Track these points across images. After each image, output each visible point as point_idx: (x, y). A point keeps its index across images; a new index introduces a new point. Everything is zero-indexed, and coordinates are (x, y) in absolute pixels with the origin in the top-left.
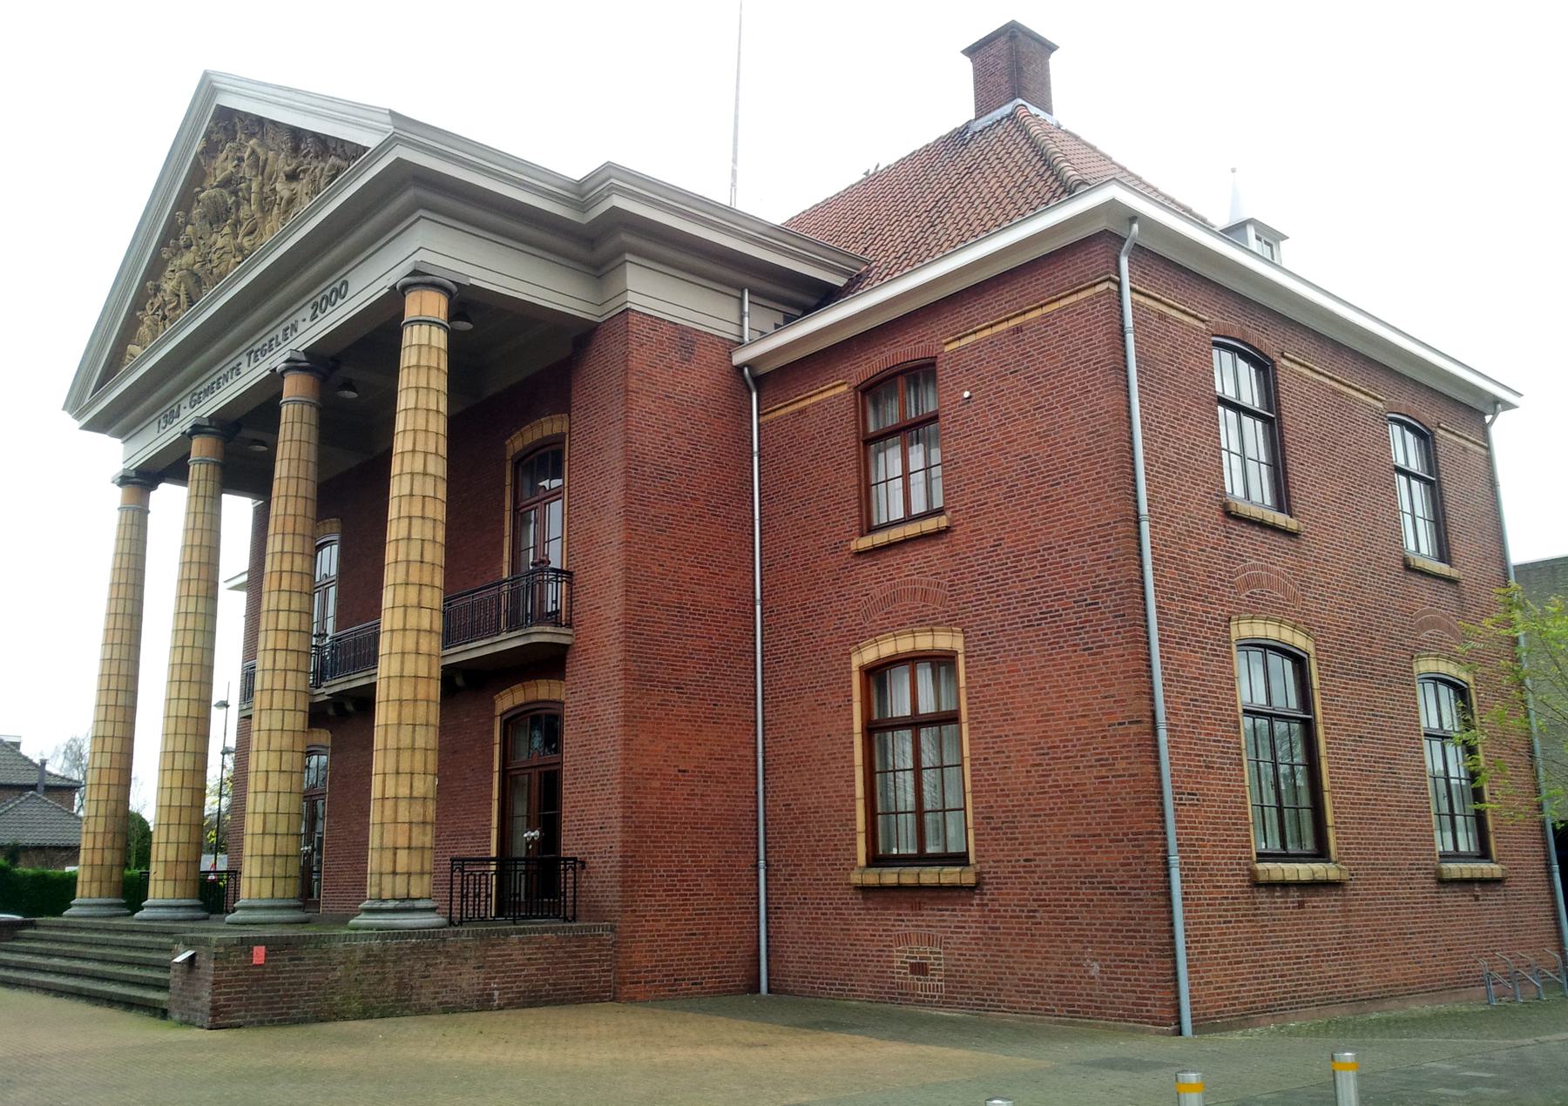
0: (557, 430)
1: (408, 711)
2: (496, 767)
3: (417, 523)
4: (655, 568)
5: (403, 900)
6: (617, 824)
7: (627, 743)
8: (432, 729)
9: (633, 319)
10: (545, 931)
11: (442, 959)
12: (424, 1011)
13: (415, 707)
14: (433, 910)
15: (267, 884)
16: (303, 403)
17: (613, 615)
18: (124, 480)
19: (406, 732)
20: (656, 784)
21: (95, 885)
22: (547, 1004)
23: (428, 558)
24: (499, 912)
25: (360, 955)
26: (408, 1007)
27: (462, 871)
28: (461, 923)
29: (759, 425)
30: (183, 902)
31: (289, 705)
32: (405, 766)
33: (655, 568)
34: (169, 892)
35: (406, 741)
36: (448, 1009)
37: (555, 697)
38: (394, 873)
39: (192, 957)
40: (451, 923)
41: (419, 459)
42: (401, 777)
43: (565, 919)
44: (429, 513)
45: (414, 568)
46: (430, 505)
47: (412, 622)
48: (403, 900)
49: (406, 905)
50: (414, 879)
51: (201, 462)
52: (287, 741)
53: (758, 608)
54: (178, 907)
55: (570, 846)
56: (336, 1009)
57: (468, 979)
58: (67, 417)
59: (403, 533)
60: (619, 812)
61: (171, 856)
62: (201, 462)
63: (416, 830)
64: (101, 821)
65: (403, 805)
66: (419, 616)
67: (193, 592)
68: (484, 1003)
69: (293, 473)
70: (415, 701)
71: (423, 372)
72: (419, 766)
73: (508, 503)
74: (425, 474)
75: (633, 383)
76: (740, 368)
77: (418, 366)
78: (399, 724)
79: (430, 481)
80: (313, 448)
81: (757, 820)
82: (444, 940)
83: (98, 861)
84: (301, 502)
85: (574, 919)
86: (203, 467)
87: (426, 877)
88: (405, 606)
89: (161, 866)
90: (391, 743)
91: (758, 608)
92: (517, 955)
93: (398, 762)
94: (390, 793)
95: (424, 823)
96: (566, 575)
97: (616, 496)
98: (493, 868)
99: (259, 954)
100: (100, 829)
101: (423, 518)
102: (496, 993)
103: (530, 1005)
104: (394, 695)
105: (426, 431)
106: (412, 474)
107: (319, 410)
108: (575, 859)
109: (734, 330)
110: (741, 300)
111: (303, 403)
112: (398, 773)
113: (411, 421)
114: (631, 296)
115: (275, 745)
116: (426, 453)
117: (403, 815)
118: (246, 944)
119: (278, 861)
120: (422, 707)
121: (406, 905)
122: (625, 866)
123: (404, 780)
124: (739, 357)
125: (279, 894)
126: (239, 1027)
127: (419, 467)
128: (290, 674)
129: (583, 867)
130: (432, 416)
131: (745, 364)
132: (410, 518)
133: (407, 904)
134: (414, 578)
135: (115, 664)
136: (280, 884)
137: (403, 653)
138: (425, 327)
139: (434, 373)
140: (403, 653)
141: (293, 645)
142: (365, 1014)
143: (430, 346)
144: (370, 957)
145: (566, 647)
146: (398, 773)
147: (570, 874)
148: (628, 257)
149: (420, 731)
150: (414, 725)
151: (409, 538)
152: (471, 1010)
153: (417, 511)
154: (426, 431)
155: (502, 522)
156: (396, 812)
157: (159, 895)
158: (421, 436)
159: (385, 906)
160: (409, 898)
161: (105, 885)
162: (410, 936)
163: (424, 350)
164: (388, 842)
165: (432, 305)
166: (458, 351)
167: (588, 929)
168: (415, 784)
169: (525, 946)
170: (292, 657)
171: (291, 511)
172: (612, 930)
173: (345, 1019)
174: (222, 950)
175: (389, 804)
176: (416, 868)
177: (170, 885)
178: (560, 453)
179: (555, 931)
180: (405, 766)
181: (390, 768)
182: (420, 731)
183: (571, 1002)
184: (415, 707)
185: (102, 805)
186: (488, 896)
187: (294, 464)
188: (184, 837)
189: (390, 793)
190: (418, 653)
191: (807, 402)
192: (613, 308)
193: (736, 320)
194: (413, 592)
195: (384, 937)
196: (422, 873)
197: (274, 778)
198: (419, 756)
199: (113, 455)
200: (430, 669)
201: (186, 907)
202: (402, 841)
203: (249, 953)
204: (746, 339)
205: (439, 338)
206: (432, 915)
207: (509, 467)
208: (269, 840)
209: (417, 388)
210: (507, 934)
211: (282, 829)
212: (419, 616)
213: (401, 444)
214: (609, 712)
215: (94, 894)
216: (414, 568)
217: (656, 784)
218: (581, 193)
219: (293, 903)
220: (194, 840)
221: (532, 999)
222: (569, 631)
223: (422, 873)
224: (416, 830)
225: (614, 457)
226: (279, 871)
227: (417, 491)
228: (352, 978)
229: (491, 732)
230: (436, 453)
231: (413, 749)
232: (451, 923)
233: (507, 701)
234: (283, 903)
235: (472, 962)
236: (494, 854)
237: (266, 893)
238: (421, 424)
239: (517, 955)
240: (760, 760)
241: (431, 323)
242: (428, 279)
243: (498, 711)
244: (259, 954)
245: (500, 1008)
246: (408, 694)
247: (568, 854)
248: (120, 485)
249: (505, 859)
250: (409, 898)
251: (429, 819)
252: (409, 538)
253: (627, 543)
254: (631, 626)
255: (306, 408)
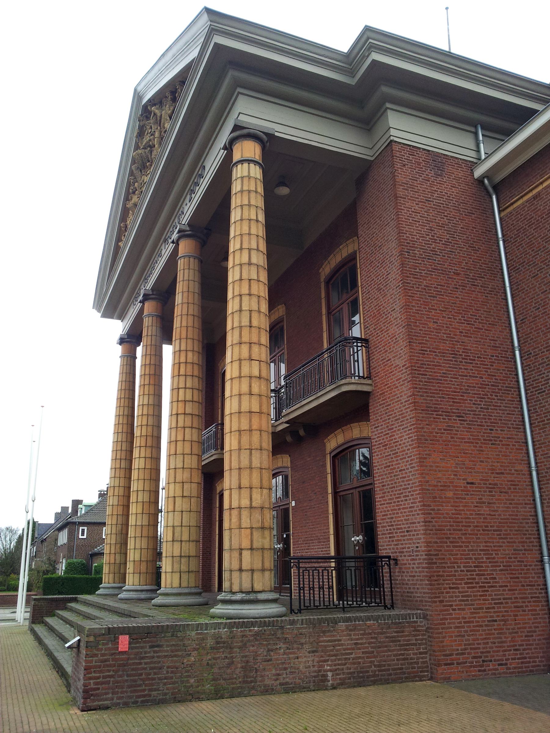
0: (350, 251)
1: (245, 438)
2: (330, 490)
3: (245, 299)
4: (431, 325)
5: (248, 593)
6: (420, 527)
7: (422, 460)
8: (265, 453)
9: (396, 147)
10: (370, 618)
11: (282, 645)
12: (268, 691)
13: (251, 436)
14: (274, 601)
15: (176, 576)
16: (189, 257)
17: (400, 362)
18: (122, 341)
19: (245, 455)
20: (450, 494)
21: (111, 576)
22: (374, 683)
23: (255, 323)
24: (340, 598)
25: (210, 642)
26: (253, 688)
27: (299, 568)
28: (300, 611)
29: (501, 219)
30: (145, 587)
31: (187, 450)
32: (245, 482)
33: (431, 325)
34: (137, 582)
35: (245, 462)
36: (289, 689)
37: (365, 434)
38: (241, 570)
39: (79, 640)
40: (292, 611)
41: (245, 254)
42: (243, 491)
43: (385, 607)
44: (254, 291)
45: (246, 331)
46: (254, 285)
47: (246, 371)
48: (248, 593)
49: (251, 597)
50: (256, 575)
51: (149, 316)
52: (187, 475)
53: (517, 353)
54: (142, 591)
55: (385, 547)
56: (191, 690)
57: (305, 662)
58: (95, 311)
59: (237, 307)
60: (420, 518)
61: (137, 558)
62: (149, 316)
63: (256, 534)
64: (114, 537)
65: (245, 514)
66: (250, 366)
67: (146, 392)
68: (319, 684)
69: (185, 300)
70: (251, 430)
71: (245, 195)
72: (256, 482)
73: (324, 311)
74: (250, 264)
75: (400, 192)
76: (480, 181)
77: (242, 191)
78: (240, 449)
79: (254, 270)
80: (197, 285)
81: (537, 523)
82: (282, 628)
83: (112, 561)
84: (191, 318)
85: (392, 607)
86: (151, 318)
87: (267, 574)
88: (240, 360)
89: (132, 564)
90: (235, 465)
91: (517, 353)
92: (345, 640)
93: (240, 479)
94: (235, 504)
95: (263, 528)
96: (365, 341)
97: (394, 273)
98: (333, 564)
99: (124, 642)
100: (113, 542)
101: (250, 295)
102: (330, 674)
103: (360, 684)
104: (235, 427)
105: (249, 234)
106: (241, 265)
107: (201, 262)
108: (389, 557)
109: (473, 154)
110: (476, 134)
111: (189, 257)
112: (240, 488)
113: (238, 228)
114: (393, 132)
115: (179, 479)
116: (250, 250)
117: (246, 522)
118: (113, 633)
119: (183, 560)
120: (256, 436)
121: (251, 597)
122: (431, 563)
123: (245, 493)
124: (478, 172)
125: (184, 584)
126: (107, 708)
127: (245, 259)
128: (187, 430)
129: (396, 564)
130: (253, 224)
131: (483, 176)
132: (241, 295)
133: (252, 597)
134: (245, 339)
135: (119, 444)
136: (185, 576)
137: (240, 395)
138: (246, 165)
139: (253, 195)
140: (240, 395)
141: (188, 411)
142: (217, 695)
143: (249, 177)
144: (219, 643)
145: (368, 394)
146: (240, 488)
147: (386, 569)
148: (388, 105)
149: (256, 455)
150: (251, 450)
151: (241, 310)
152: (309, 690)
153: (245, 291)
154: (249, 234)
155: (321, 323)
156: (240, 519)
157: (131, 583)
158: (246, 238)
159: (235, 597)
160: (253, 591)
161: (117, 575)
162: (253, 624)
163: (246, 180)
164: (236, 545)
165: (249, 149)
166: (270, 183)
167: (404, 617)
168: (254, 497)
169: (353, 632)
170: (188, 420)
171: (184, 324)
172: (425, 617)
173: (199, 699)
174: (92, 639)
175: (235, 513)
176: (258, 565)
177: (137, 576)
178: (355, 265)
179: (377, 618)
180: (245, 482)
181: (235, 484)
182: (256, 455)
183: (394, 681)
184: (251, 436)
185: (114, 527)
186: (330, 587)
187: (185, 294)
188: (144, 545)
189: (235, 504)
190: (251, 394)
191: (540, 188)
192: (381, 145)
193: (473, 147)
194: (245, 349)
195: (230, 626)
196: (263, 570)
197: (179, 501)
198: (256, 474)
199: (117, 327)
200: (260, 406)
201: (147, 591)
202: (246, 544)
203: (115, 641)
204: (483, 157)
205: (256, 172)
206: (273, 605)
207: (323, 285)
208: (177, 545)
209: (242, 206)
210: (335, 622)
211: (185, 537)
212: (250, 366)
213: (234, 245)
214: (405, 438)
215: (111, 581)
216: (246, 331)
217: (450, 494)
218: (349, 61)
219: (193, 590)
220: (151, 546)
221: (360, 679)
222: (369, 382)
223: (263, 570)
224: (256, 534)
225: (391, 248)
226: (184, 568)
227: (245, 276)
228: (205, 662)
229: (324, 466)
230: (258, 250)
231: (251, 468)
232: (292, 611)
233: (333, 442)
234: (186, 591)
235: (306, 646)
236: (333, 553)
237: (176, 583)
238: (245, 230)
239: (345, 640)
240: (534, 474)
241: (249, 161)
242: (245, 131)
243: (328, 451)
244: (124, 642)
245: (334, 688)
246: (245, 426)
247: (383, 553)
248: (120, 344)
249: (340, 558)
250: (253, 591)
251: (267, 525)
252: (241, 310)
253: (407, 307)
254: (416, 369)
255: (192, 260)
